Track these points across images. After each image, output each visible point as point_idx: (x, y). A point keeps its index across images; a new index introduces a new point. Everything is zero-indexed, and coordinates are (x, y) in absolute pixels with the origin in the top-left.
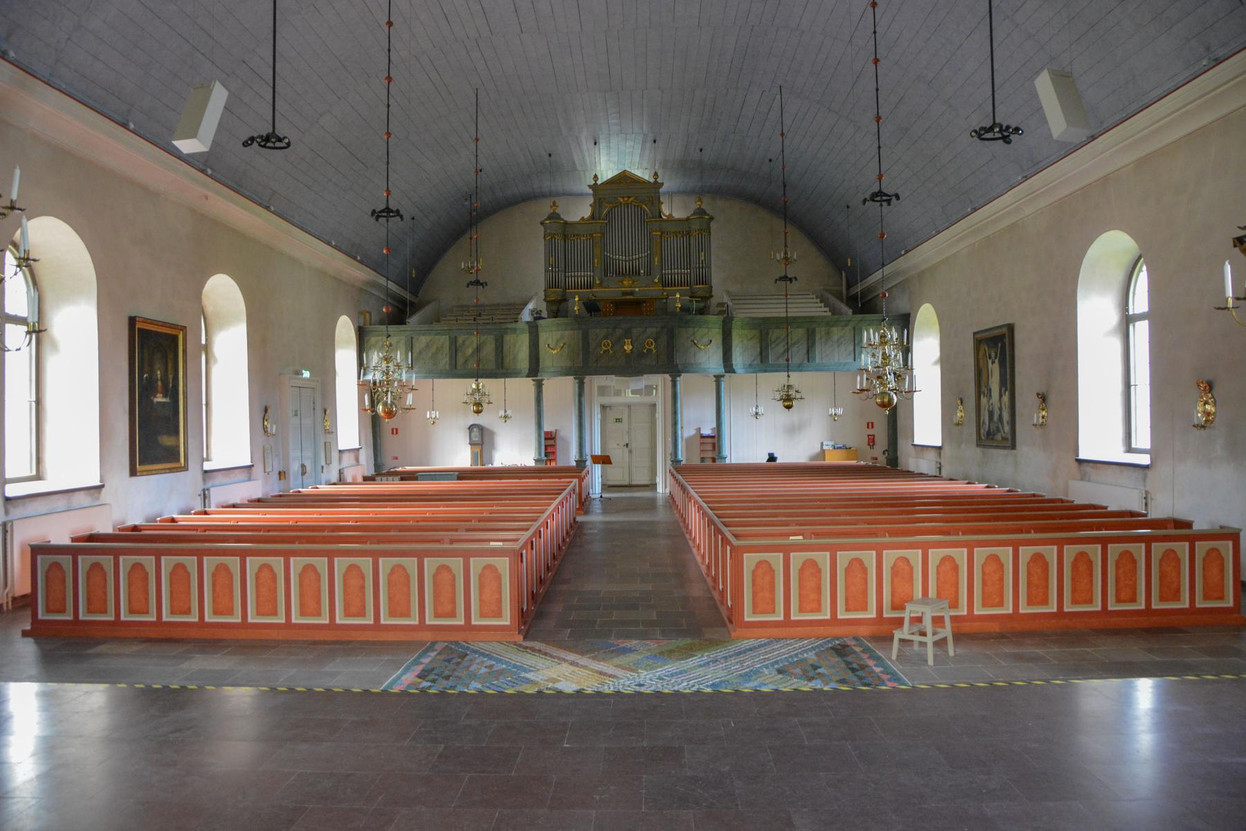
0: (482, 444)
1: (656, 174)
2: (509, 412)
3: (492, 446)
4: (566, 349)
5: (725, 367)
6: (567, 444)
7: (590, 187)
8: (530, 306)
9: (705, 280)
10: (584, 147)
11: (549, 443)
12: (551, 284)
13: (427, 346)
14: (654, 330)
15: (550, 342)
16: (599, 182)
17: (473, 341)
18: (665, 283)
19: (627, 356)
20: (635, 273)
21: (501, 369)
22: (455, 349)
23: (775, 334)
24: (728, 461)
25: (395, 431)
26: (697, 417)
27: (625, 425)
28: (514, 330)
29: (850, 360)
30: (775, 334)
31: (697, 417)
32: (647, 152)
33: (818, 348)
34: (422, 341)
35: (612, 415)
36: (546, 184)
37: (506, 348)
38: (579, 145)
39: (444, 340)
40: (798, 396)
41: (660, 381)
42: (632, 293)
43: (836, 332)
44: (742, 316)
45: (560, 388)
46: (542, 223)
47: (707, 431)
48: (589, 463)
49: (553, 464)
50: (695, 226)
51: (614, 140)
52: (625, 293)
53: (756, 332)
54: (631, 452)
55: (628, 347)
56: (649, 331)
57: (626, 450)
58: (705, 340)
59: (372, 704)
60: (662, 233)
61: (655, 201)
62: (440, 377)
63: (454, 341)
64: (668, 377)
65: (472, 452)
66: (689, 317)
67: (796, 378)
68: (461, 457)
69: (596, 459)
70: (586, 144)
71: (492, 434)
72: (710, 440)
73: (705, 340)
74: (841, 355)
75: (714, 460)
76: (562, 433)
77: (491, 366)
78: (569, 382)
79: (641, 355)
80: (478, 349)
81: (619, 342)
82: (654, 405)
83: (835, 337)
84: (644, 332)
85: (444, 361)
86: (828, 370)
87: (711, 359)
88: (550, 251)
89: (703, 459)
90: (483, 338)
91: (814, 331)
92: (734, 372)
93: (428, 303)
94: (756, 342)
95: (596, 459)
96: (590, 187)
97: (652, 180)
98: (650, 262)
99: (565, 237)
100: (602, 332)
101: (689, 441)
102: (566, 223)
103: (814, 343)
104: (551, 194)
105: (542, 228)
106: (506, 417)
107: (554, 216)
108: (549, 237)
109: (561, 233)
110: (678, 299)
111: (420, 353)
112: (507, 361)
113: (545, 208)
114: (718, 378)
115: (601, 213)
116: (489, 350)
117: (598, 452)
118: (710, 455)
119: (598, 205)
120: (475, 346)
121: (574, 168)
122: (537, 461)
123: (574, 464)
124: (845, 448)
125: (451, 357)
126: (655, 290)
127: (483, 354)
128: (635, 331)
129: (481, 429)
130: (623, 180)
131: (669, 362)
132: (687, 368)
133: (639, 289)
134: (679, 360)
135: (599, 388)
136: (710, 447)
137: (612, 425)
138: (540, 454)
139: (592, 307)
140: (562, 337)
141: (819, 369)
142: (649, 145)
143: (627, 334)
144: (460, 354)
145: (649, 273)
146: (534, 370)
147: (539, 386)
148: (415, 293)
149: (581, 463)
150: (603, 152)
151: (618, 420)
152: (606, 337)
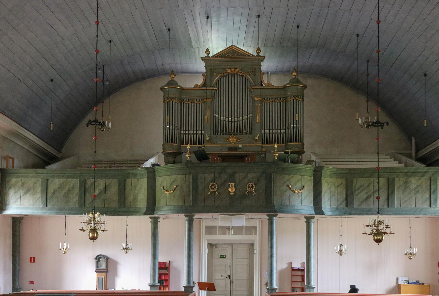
0: (106, 272)
1: (258, 49)
2: (344, 248)
3: (115, 274)
4: (178, 192)
5: (315, 209)
6: (179, 273)
7: (203, 59)
8: (152, 160)
9: (297, 138)
10: (198, 21)
11: (163, 272)
12: (169, 139)
13: (61, 187)
14: (254, 175)
15: (165, 185)
16: (211, 55)
17: (101, 184)
18: (265, 141)
19: (231, 197)
20: (238, 131)
21: (122, 207)
22: (84, 190)
23: (359, 182)
24: (315, 291)
25: (33, 260)
26: (289, 253)
27: (227, 261)
28: (135, 175)
29: (426, 205)
30: (359, 182)
31: (289, 253)
32: (252, 29)
33: (397, 194)
34: (55, 183)
35: (217, 252)
36: (165, 61)
37: (127, 191)
38: (194, 19)
39: (75, 182)
40: (388, 231)
41: (258, 220)
42: (236, 149)
43: (414, 182)
44: (331, 167)
45: (173, 225)
46: (162, 89)
47: (297, 265)
48: (196, 288)
49: (166, 290)
50: (291, 92)
51: (223, 16)
52: (230, 149)
53: (343, 181)
54: (232, 282)
55: (232, 190)
56: (250, 176)
57: (228, 281)
58: (299, 185)
59: (343, 169)
60: (263, 99)
61: (257, 71)
62: (70, 213)
63: (83, 184)
64: (264, 216)
65: (98, 278)
66: (285, 165)
67: (386, 219)
68: (89, 280)
69: (202, 286)
70: (200, 20)
71: (115, 263)
72: (299, 273)
73: (299, 185)
74: (419, 201)
75: (303, 289)
76: (174, 264)
77: (114, 205)
78: (181, 220)
79: (243, 197)
80: (106, 189)
81: (224, 184)
82: (252, 245)
83: (413, 186)
84: (246, 176)
85: (75, 199)
86: (406, 214)
87: (303, 202)
88: (168, 111)
89: (293, 289)
90: (108, 181)
91: (394, 179)
92: (323, 214)
93: (68, 157)
94: (341, 190)
95: (202, 286)
96: (203, 59)
97: (255, 54)
98: (252, 119)
99: (181, 101)
100: (210, 177)
101: (281, 273)
102: (182, 89)
103: (393, 192)
104: (173, 73)
105: (162, 93)
106: (126, 249)
107: (172, 83)
108: (168, 100)
109: (177, 98)
110: (276, 151)
111: (54, 193)
112: (128, 202)
113: (164, 81)
114: (308, 220)
115: (211, 82)
116: (114, 189)
117: (204, 280)
118: (299, 285)
119: (209, 73)
120: (102, 187)
121: (191, 45)
122: (151, 286)
123: (183, 289)
124: (417, 283)
125: (80, 198)
126: (256, 147)
127: (108, 195)
128: (238, 176)
129: (107, 259)
130: (231, 53)
131: (268, 204)
132: (283, 209)
133: (242, 144)
134: (276, 201)
135: (207, 227)
136: (299, 279)
137: (217, 261)
138: (154, 280)
139: (202, 156)
140: (175, 181)
141: (398, 213)
142: (254, 19)
143: (231, 178)
144: (88, 195)
145: (251, 132)
146: (151, 209)
147: (155, 222)
148: (59, 150)
149: (189, 288)
150: (215, 27)
151: (223, 256)
152: (213, 181)
